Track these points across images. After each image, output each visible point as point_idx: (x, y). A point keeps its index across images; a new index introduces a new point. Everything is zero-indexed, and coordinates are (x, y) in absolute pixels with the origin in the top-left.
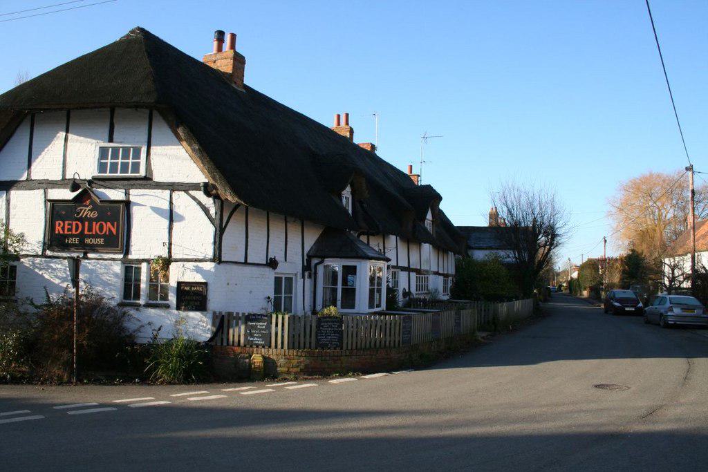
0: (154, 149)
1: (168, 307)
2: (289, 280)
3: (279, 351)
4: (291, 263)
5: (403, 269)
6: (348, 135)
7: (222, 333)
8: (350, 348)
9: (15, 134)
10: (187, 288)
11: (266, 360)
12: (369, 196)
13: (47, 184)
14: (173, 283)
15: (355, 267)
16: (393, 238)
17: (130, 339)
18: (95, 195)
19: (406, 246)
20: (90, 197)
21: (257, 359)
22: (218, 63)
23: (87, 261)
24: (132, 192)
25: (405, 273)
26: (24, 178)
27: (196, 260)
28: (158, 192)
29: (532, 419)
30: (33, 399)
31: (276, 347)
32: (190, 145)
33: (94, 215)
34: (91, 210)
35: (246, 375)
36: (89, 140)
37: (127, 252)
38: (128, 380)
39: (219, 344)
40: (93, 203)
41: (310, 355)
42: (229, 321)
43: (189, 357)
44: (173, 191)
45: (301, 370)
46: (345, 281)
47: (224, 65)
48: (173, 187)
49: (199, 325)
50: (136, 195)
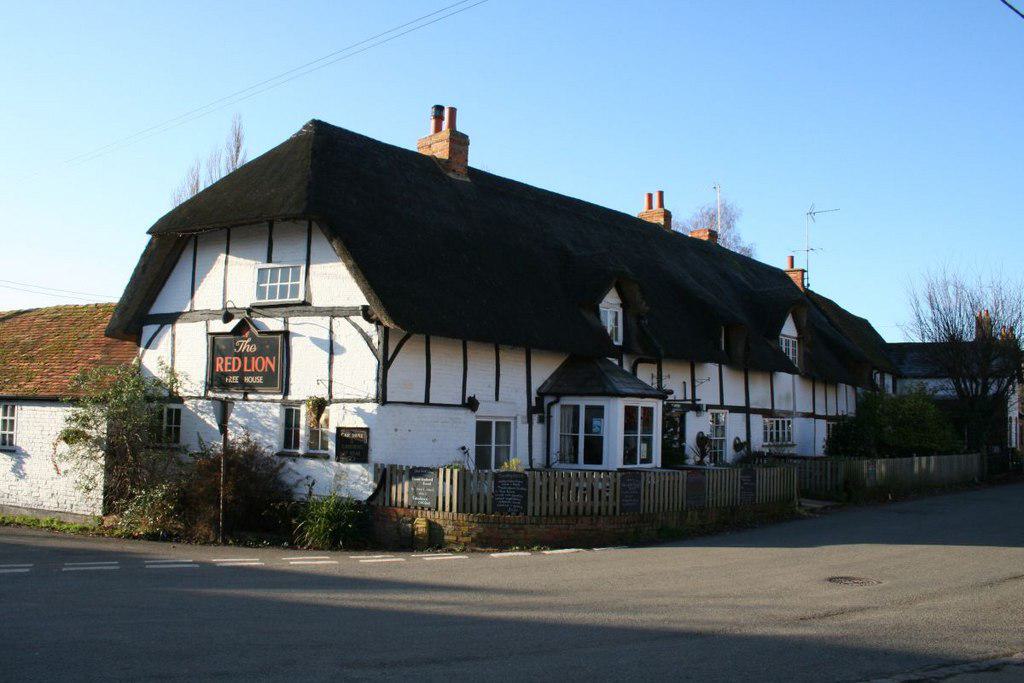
0: (313, 268)
1: (327, 457)
2: (504, 427)
3: (446, 514)
4: (505, 402)
5: (734, 409)
6: (661, 221)
7: (385, 490)
8: (537, 513)
9: (180, 260)
10: (347, 435)
11: (431, 524)
12: (647, 308)
13: (210, 315)
14: (332, 430)
15: (601, 408)
16: (712, 369)
17: (288, 494)
18: (254, 326)
19: (743, 375)
20: (249, 328)
21: (421, 525)
22: (433, 148)
23: (246, 403)
24: (292, 320)
25: (741, 417)
26: (187, 309)
27: (358, 401)
28: (317, 319)
29: (595, 607)
30: (133, 553)
31: (444, 509)
32: (345, 261)
33: (252, 349)
34: (250, 343)
35: (407, 543)
36: (248, 261)
37: (286, 392)
38: (293, 546)
39: (381, 504)
40: (252, 335)
41: (482, 521)
42: (391, 475)
43: (339, 518)
44: (333, 317)
45: (473, 540)
46: (588, 427)
47: (441, 150)
48: (333, 313)
49: (359, 481)
50: (298, 324)
